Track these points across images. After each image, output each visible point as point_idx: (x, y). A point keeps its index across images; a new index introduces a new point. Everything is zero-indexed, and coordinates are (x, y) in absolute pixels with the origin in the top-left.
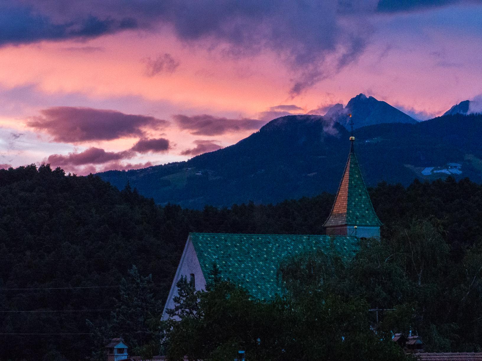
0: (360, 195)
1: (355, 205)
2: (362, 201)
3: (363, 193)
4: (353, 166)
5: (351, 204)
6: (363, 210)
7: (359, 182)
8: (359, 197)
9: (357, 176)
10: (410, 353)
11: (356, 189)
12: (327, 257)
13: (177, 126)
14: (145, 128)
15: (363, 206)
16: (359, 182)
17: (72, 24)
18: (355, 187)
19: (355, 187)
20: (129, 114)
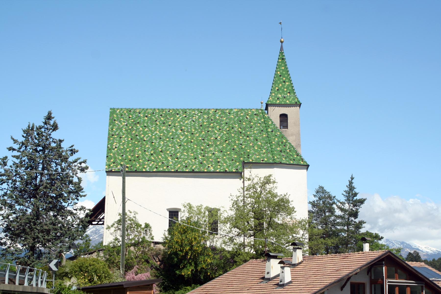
0: (284, 82)
1: (278, 90)
2: (285, 87)
3: (287, 80)
4: (280, 61)
5: (275, 89)
6: (286, 93)
7: (284, 73)
8: (283, 83)
9: (283, 68)
10: (55, 237)
11: (281, 77)
12: (292, 233)
13: (399, 250)
14: (431, 253)
15: (285, 90)
16: (284, 73)
17: (166, 109)
18: (280, 76)
19: (280, 76)
20: (275, 169)
